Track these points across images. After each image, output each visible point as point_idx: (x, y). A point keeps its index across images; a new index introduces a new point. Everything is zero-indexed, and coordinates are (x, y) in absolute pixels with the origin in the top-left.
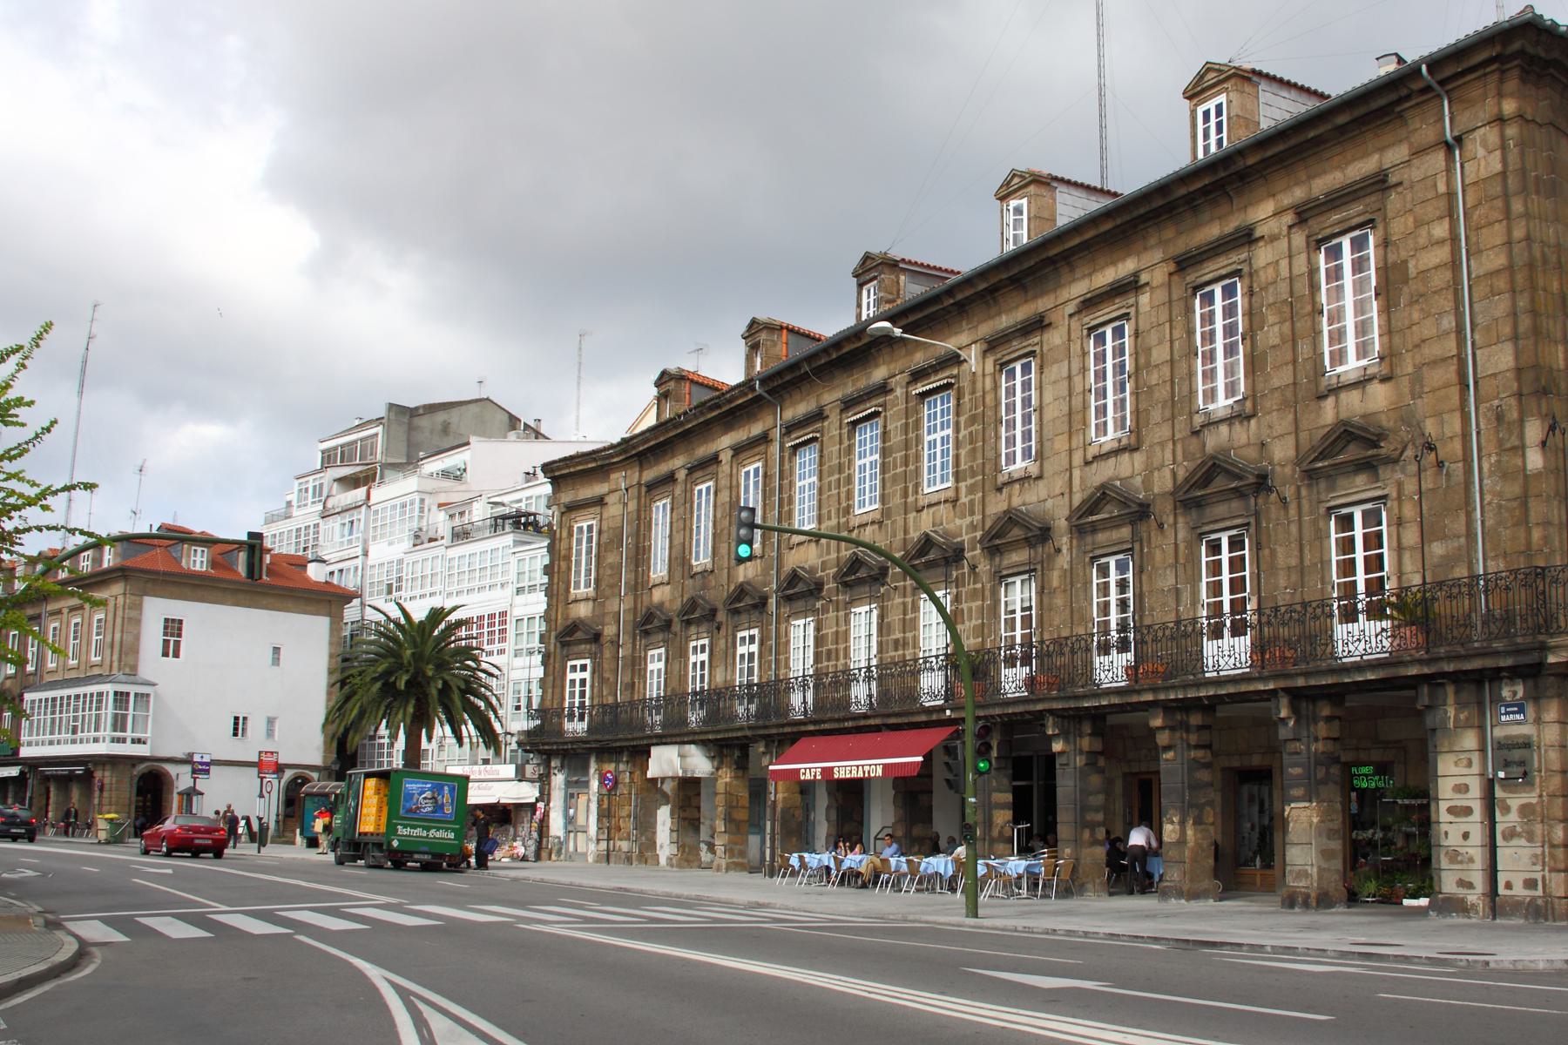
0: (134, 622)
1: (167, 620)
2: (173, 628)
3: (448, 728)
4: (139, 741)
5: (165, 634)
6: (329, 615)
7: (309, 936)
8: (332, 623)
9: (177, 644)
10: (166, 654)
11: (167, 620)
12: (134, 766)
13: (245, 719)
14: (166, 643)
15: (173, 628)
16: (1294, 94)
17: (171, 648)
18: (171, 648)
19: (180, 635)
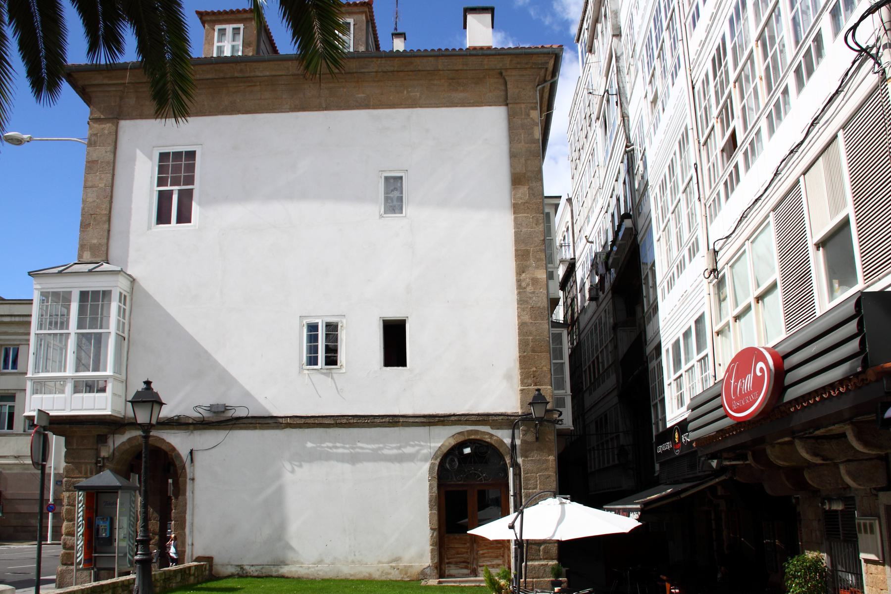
0: (103, 171)
1: (163, 156)
2: (177, 168)
3: (671, 319)
4: (92, 387)
5: (161, 182)
6: (505, 102)
7: (514, 475)
8: (511, 117)
9: (186, 198)
10: (163, 217)
11: (163, 156)
12: (102, 439)
13: (313, 361)
14: (164, 199)
15: (177, 168)
16: (789, 350)
17: (173, 208)
18: (173, 208)
19: (190, 180)
